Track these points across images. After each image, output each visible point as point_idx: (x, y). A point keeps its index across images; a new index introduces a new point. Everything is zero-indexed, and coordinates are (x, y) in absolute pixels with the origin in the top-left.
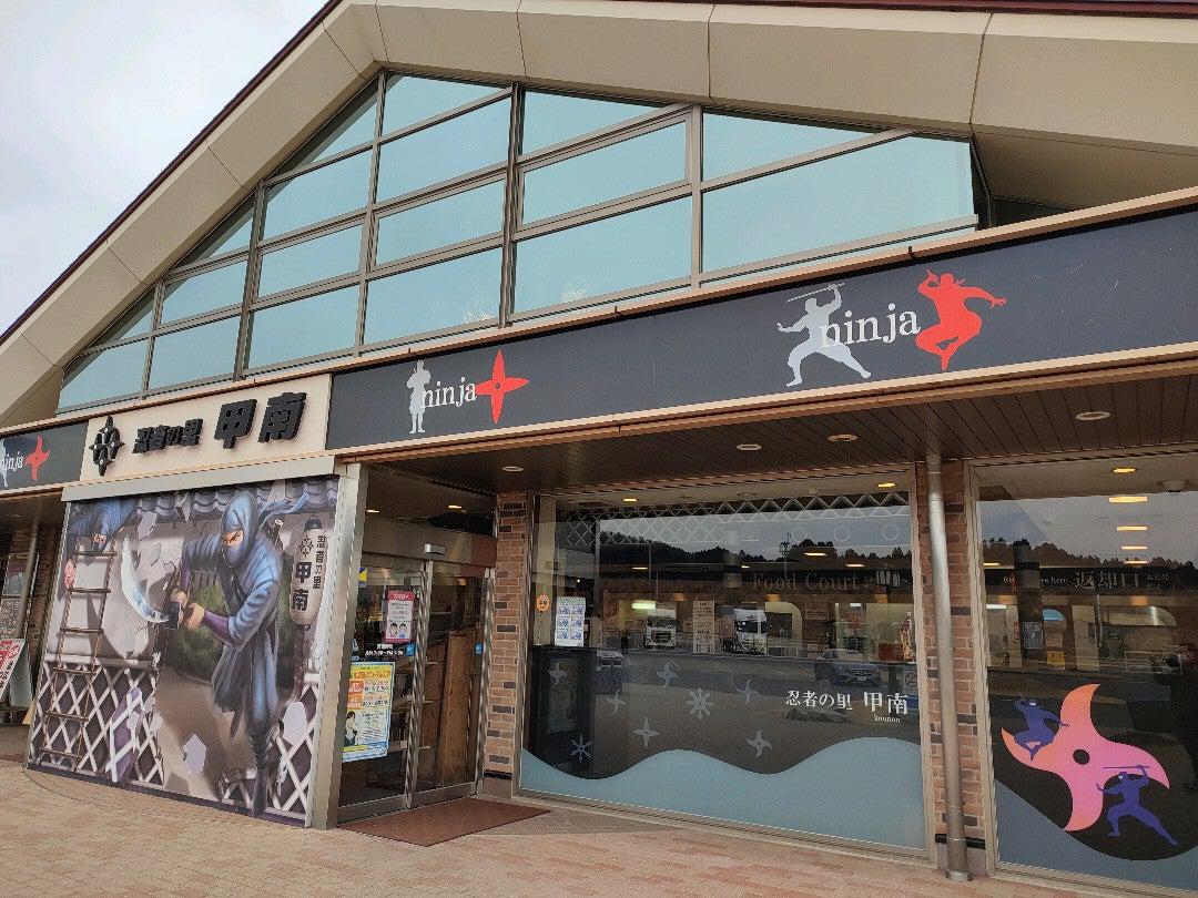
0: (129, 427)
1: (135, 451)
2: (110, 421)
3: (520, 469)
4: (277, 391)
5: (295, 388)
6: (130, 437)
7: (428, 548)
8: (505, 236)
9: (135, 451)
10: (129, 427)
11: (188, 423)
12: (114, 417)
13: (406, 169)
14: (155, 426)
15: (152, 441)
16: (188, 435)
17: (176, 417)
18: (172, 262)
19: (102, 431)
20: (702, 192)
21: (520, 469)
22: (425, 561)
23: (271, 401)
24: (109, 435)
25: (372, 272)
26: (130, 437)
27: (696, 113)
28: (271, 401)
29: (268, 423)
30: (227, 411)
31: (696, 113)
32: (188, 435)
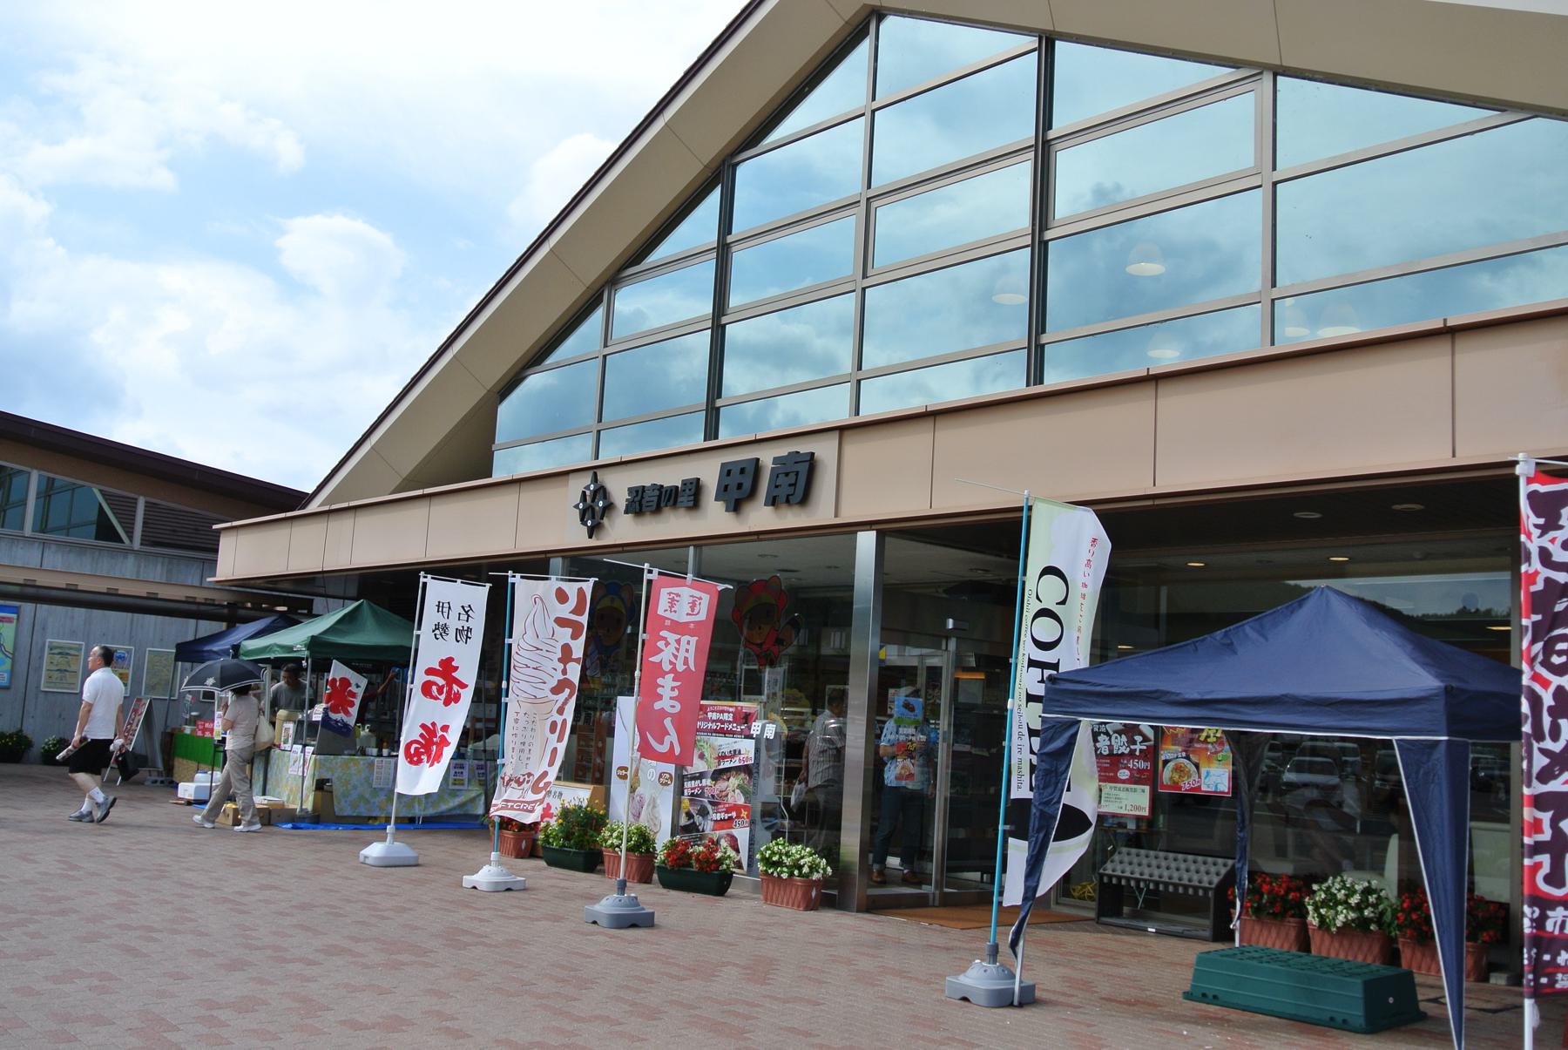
0: (619, 487)
1: (626, 512)
2: (595, 479)
3: (1318, 516)
4: (783, 450)
5: (803, 447)
6: (620, 497)
7: (950, 623)
8: (1033, 234)
9: (626, 512)
10: (619, 487)
11: (684, 483)
12: (599, 472)
13: (908, 145)
14: (648, 484)
15: (646, 502)
16: (689, 496)
17: (671, 476)
18: (622, 261)
19: (588, 487)
20: (1275, 184)
21: (1318, 516)
22: (947, 638)
23: (776, 460)
24: (595, 492)
25: (868, 204)
26: (620, 497)
27: (1267, 78)
28: (776, 460)
29: (774, 485)
30: (726, 471)
31: (1267, 78)
32: (689, 496)
